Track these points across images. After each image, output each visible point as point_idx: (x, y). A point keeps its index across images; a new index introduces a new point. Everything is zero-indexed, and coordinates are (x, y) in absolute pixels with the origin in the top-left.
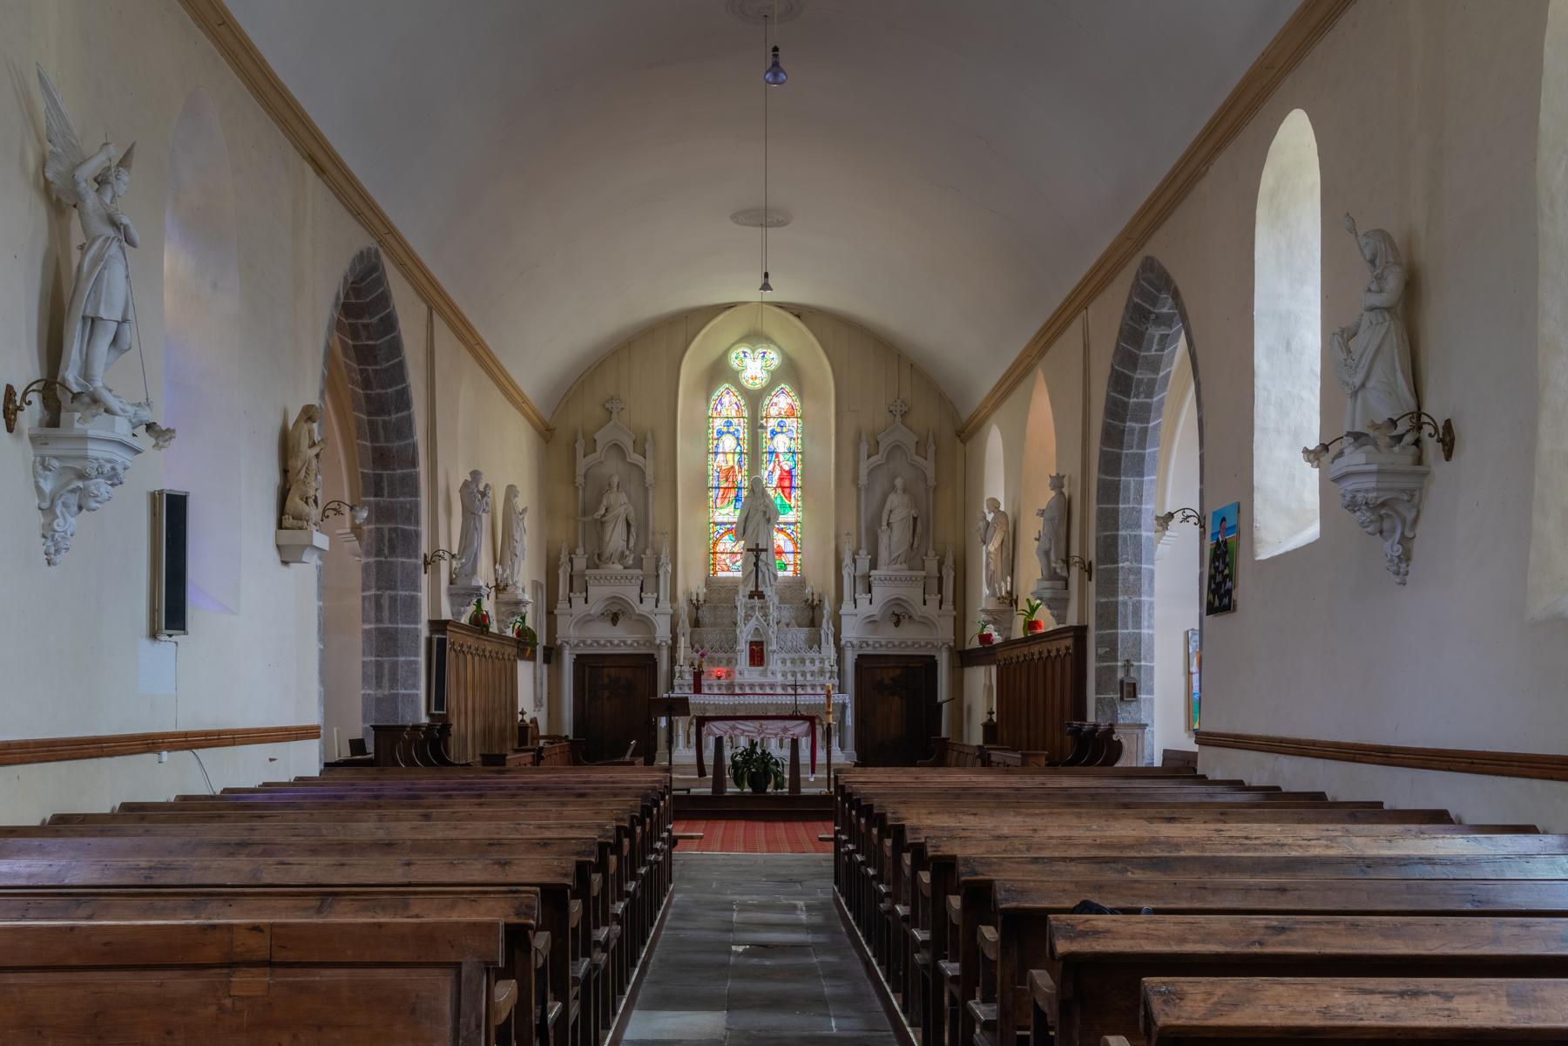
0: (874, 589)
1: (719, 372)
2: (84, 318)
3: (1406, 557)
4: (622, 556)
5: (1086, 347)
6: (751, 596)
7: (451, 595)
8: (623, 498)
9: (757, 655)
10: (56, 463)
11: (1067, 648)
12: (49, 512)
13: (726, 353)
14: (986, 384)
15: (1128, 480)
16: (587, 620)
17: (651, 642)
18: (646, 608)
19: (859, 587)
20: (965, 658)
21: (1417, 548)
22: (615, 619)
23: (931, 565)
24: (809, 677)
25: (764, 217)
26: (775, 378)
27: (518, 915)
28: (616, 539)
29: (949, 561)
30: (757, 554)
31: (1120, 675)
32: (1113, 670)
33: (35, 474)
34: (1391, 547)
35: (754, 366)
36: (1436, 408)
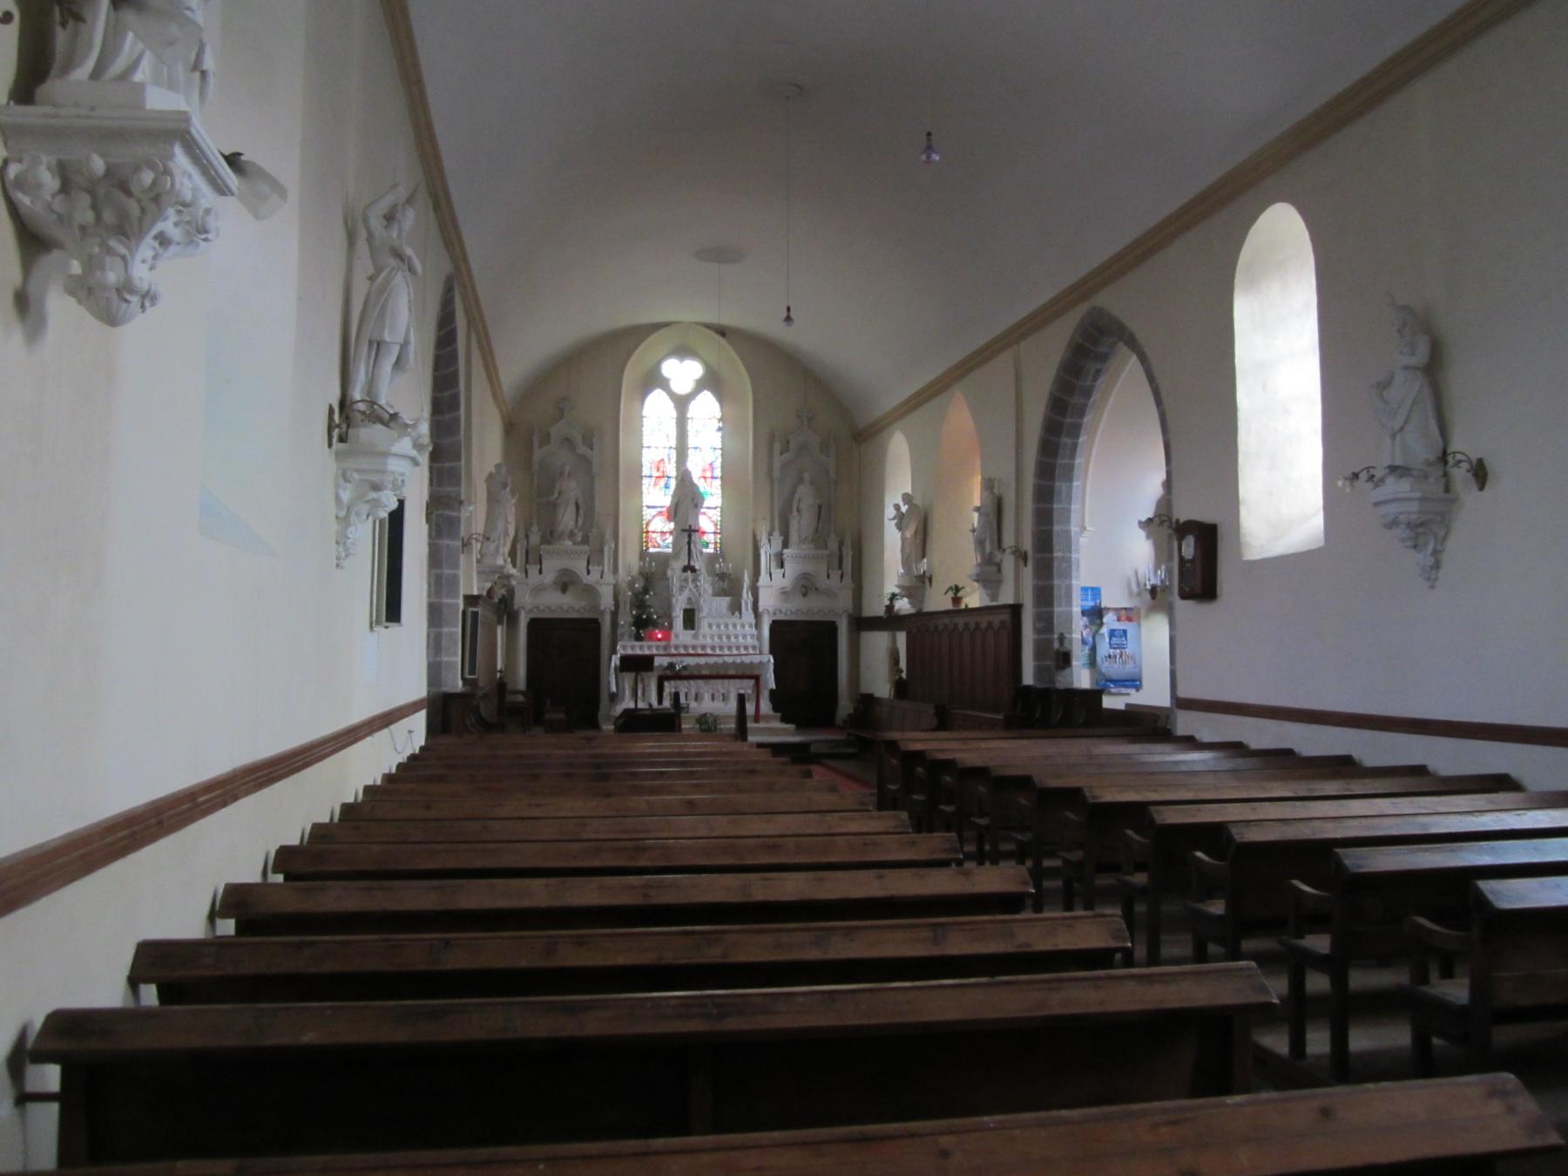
0: (786, 565)
1: (653, 380)
2: (371, 342)
3: (1437, 566)
4: (572, 535)
5: (1018, 378)
6: (685, 569)
7: (479, 573)
8: (573, 484)
9: (690, 619)
10: (356, 476)
11: (1002, 622)
12: (344, 521)
13: (659, 363)
14: (891, 400)
15: (1060, 485)
16: (538, 590)
17: (596, 608)
18: (587, 579)
19: (773, 564)
20: (862, 624)
21: (1445, 557)
22: (564, 588)
23: (833, 544)
24: (741, 639)
25: (720, 255)
26: (701, 385)
27: (1115, 938)
28: (567, 519)
29: (848, 542)
30: (687, 533)
31: (1056, 645)
32: (1050, 641)
33: (337, 486)
34: (1424, 557)
35: (682, 372)
36: (1461, 443)
